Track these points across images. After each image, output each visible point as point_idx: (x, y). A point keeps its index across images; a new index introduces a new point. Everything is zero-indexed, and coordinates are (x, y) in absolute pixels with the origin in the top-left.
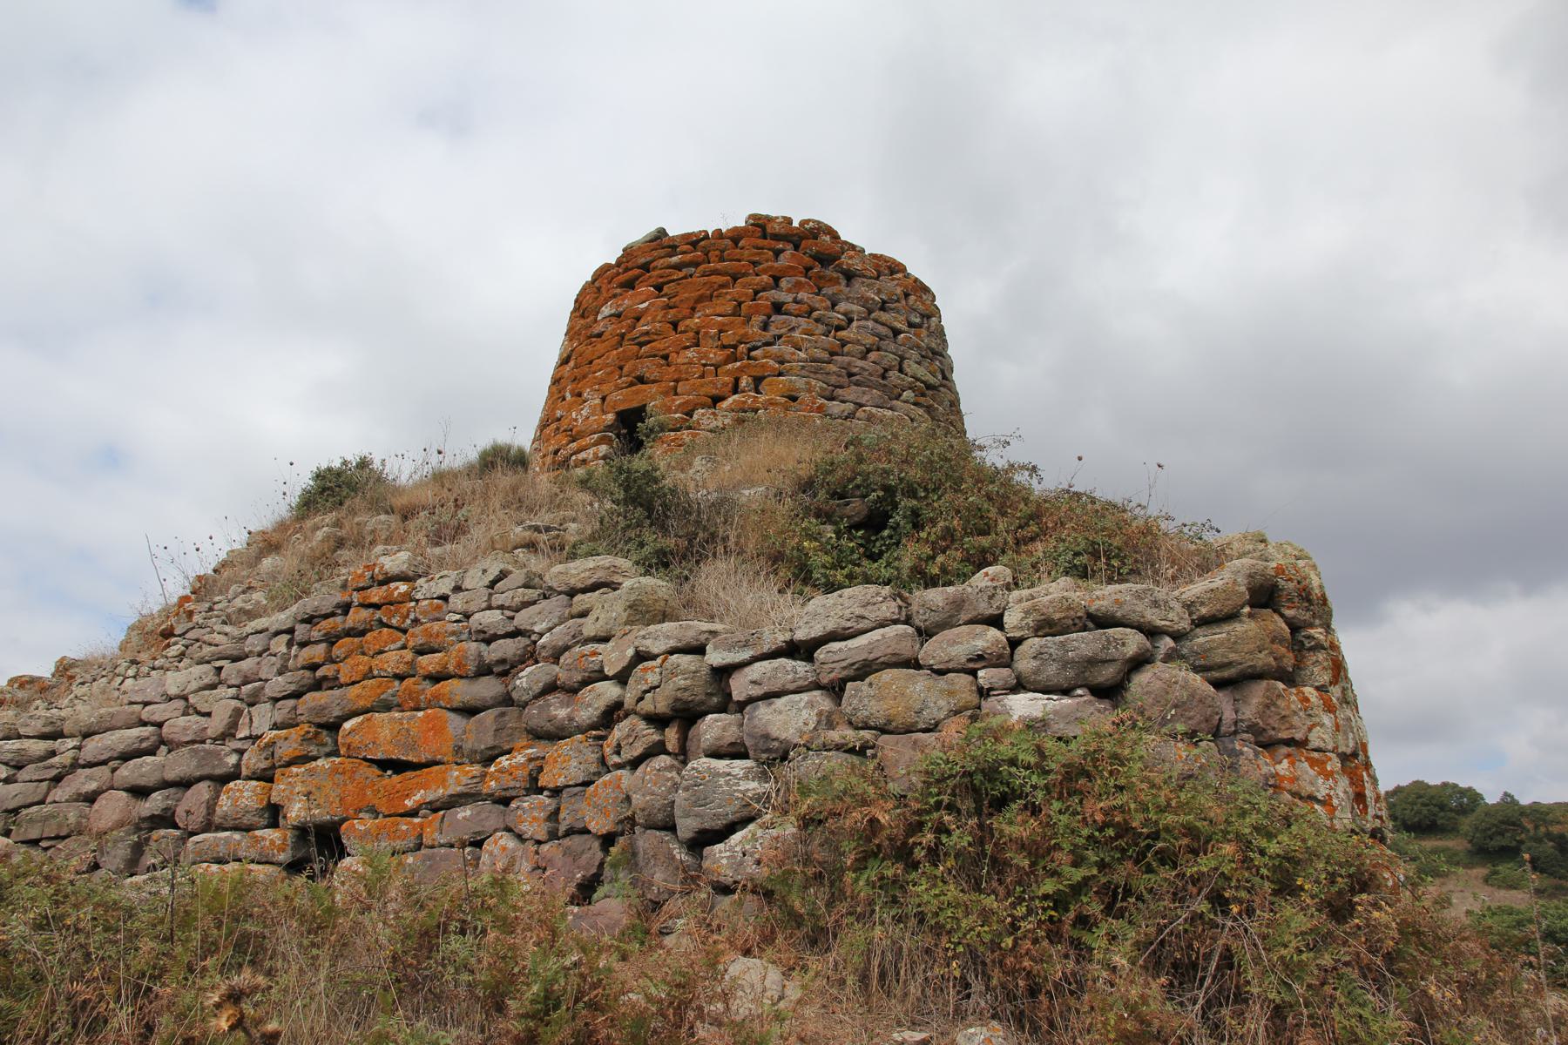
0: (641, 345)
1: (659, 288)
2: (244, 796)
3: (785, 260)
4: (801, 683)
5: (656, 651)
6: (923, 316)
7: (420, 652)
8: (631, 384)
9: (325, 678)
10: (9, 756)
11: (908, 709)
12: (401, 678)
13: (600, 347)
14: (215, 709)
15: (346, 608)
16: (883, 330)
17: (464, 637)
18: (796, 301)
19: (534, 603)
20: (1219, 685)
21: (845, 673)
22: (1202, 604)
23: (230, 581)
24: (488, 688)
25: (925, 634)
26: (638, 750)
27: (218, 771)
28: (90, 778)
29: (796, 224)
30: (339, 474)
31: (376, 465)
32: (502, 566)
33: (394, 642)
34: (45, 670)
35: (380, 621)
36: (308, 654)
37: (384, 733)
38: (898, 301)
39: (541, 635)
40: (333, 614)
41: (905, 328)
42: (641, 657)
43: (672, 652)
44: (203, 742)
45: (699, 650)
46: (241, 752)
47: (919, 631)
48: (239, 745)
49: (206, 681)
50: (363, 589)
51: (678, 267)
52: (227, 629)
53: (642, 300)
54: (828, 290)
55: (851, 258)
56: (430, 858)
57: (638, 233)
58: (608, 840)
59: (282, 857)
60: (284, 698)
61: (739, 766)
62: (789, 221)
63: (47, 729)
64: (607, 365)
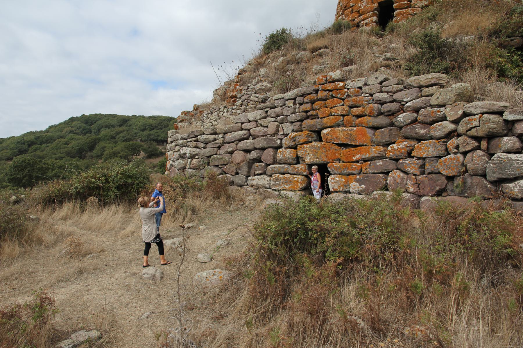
2: (286, 153)
5: (476, 113)
7: (351, 107)
9: (311, 115)
10: (203, 140)
12: (343, 116)
14: (269, 124)
15: (317, 91)
17: (370, 102)
19: (401, 90)
24: (382, 120)
26: (468, 148)
27: (275, 145)
28: (230, 147)
30: (277, 36)
32: (385, 77)
33: (339, 103)
34: (191, 109)
35: (332, 96)
37: (341, 134)
39: (407, 102)
40: (311, 93)
42: (465, 115)
43: (483, 113)
44: (266, 136)
46: (281, 139)
48: (280, 137)
49: (263, 116)
50: (323, 84)
52: (257, 95)
58: (450, 179)
59: (305, 174)
60: (296, 122)
63: (212, 132)
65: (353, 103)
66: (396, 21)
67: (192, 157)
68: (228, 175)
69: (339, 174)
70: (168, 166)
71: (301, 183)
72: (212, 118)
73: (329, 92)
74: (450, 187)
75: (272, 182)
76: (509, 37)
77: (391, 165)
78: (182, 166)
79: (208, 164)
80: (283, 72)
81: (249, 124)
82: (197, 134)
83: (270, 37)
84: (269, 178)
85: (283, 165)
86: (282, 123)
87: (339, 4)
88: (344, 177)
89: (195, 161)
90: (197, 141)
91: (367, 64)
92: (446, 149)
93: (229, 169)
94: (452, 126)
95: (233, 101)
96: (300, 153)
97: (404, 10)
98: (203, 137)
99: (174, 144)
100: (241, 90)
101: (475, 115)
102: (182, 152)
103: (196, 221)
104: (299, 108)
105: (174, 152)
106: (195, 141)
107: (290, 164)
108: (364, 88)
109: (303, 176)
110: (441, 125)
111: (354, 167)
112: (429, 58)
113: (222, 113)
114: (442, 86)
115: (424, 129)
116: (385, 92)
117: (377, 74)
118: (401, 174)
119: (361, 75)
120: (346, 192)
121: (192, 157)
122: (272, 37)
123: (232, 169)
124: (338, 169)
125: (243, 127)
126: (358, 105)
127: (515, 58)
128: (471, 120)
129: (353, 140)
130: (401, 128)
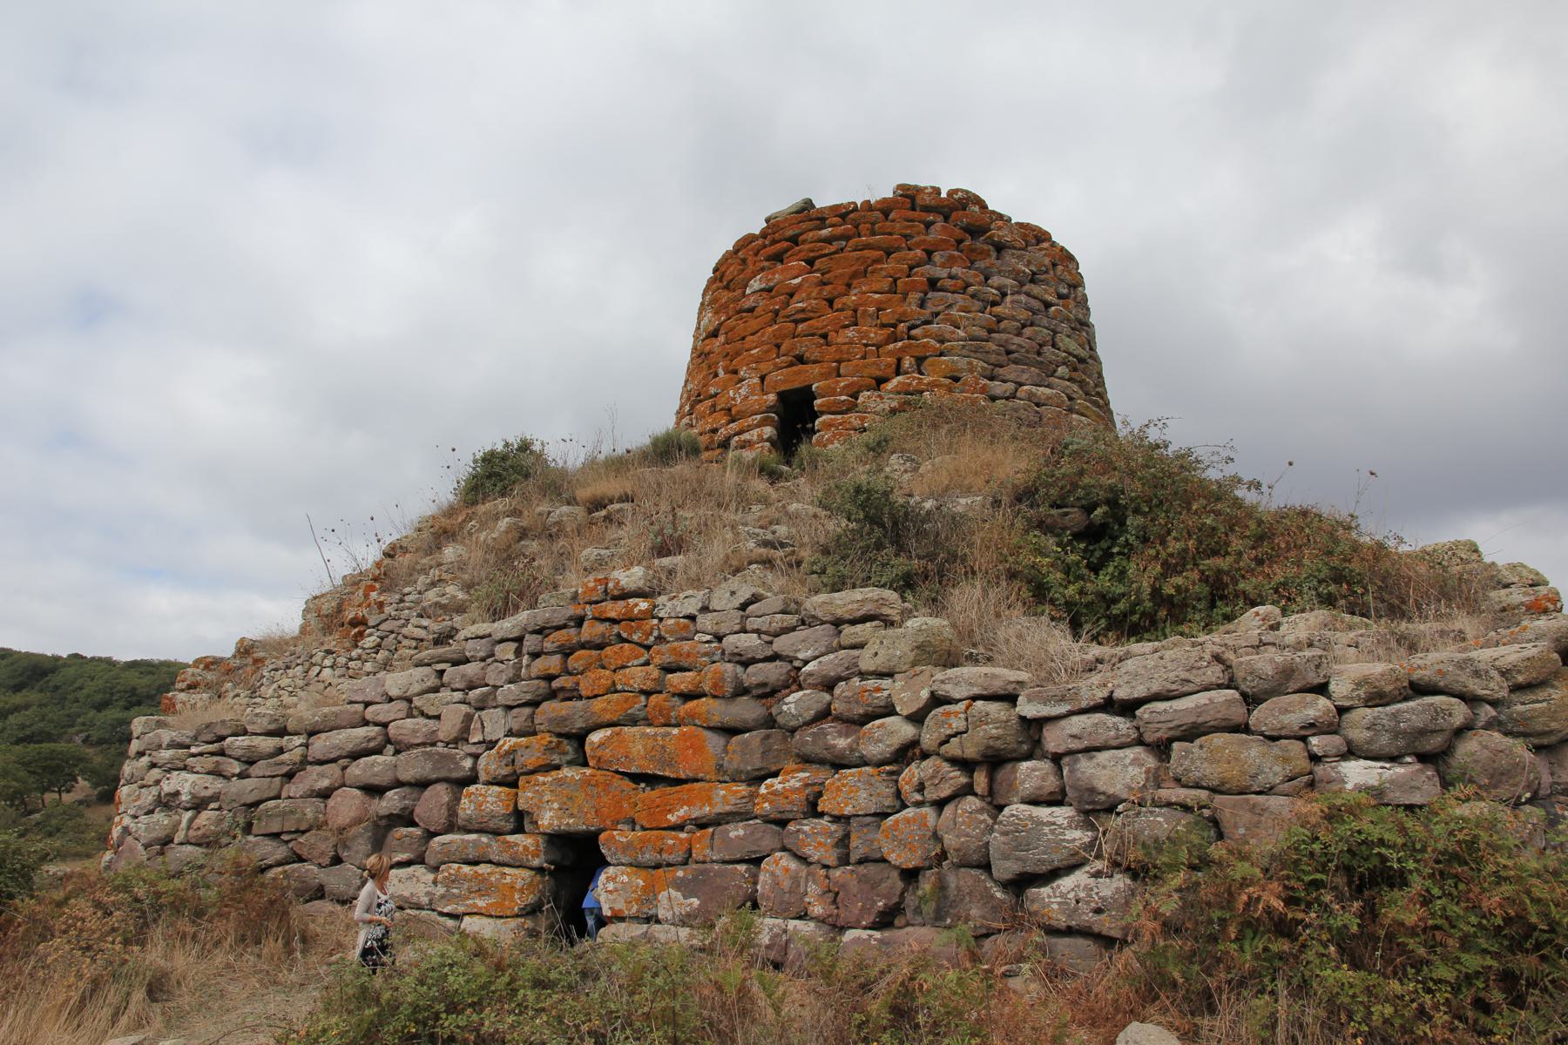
0: (797, 322)
1: (810, 262)
2: (486, 800)
3: (938, 232)
4: (1123, 740)
5: (958, 696)
6: (1070, 286)
7: (668, 669)
8: (791, 365)
9: (562, 689)
10: (240, 752)
11: (1243, 773)
12: (648, 694)
13: (754, 324)
14: (444, 711)
15: (579, 621)
16: (1036, 304)
17: (716, 658)
18: (951, 277)
19: (793, 629)
20: (1538, 749)
21: (1171, 733)
22: (1519, 672)
23: (414, 571)
24: (746, 709)
25: (1252, 700)
26: (945, 791)
27: (455, 775)
28: (322, 775)
29: (944, 195)
30: (504, 458)
31: (537, 447)
32: (754, 590)
33: (637, 657)
35: (619, 635)
36: (540, 665)
37: (637, 746)
38: (1046, 272)
39: (806, 662)
40: (565, 626)
41: (1055, 300)
42: (937, 701)
43: (974, 698)
44: (434, 744)
45: (1011, 699)
46: (476, 757)
47: (1244, 695)
48: (473, 749)
49: (429, 684)
50: (597, 602)
51: (828, 240)
52: (425, 622)
53: (792, 273)
54: (981, 264)
55: (999, 228)
56: (702, 872)
57: (783, 203)
58: (910, 876)
59: (536, 862)
60: (518, 706)
61: (1062, 814)
62: (937, 191)
63: (272, 727)
64: (763, 343)
65: (672, 659)
66: (819, 443)
67: (199, 805)
68: (307, 866)
69: (631, 865)
70: (116, 832)
71: (521, 891)
72: (285, 682)
73: (612, 624)
74: (911, 901)
75: (441, 890)
76: (1059, 507)
77: (767, 838)
78: (161, 834)
79: (248, 829)
80: (504, 561)
81: (386, 706)
82: (224, 732)
83: (484, 460)
84: (431, 877)
85: (474, 836)
86: (482, 709)
88: (643, 872)
89: (206, 816)
90: (222, 753)
91: (716, 551)
92: (898, 794)
93: (312, 847)
94: (908, 731)
95: (356, 635)
96: (526, 798)
98: (243, 741)
99: (145, 760)
100: (381, 605)
101: (958, 701)
102: (167, 787)
103: (158, 1022)
104: (528, 666)
105: (142, 787)
106: (212, 754)
107: (497, 833)
108: (699, 619)
109: (531, 869)
110: (882, 725)
111: (671, 842)
112: (868, 547)
113: (316, 669)
114: (888, 623)
115: (847, 736)
116: (753, 631)
117: (734, 583)
118: (793, 865)
119: (696, 583)
120: (648, 920)
121: (199, 805)
122: (489, 458)
123: (323, 846)
124: (626, 848)
125: (368, 717)
126: (686, 665)
127: (1073, 558)
128: (948, 714)
129: (670, 765)
130: (793, 731)
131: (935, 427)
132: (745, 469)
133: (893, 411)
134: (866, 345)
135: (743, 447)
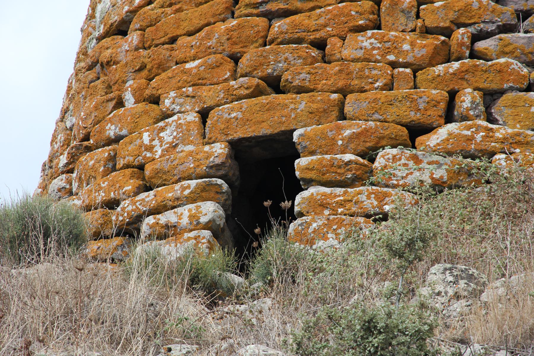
8: (257, 93)
64: (209, 51)
66: (301, 236)
87: (62, 119)
97: (339, 191)
131: (514, 218)
132: (165, 277)
133: (438, 186)
134: (394, 65)
135: (161, 237)
